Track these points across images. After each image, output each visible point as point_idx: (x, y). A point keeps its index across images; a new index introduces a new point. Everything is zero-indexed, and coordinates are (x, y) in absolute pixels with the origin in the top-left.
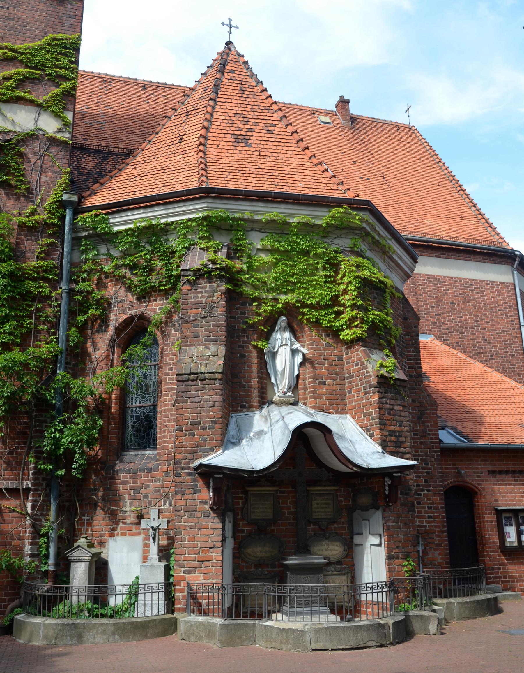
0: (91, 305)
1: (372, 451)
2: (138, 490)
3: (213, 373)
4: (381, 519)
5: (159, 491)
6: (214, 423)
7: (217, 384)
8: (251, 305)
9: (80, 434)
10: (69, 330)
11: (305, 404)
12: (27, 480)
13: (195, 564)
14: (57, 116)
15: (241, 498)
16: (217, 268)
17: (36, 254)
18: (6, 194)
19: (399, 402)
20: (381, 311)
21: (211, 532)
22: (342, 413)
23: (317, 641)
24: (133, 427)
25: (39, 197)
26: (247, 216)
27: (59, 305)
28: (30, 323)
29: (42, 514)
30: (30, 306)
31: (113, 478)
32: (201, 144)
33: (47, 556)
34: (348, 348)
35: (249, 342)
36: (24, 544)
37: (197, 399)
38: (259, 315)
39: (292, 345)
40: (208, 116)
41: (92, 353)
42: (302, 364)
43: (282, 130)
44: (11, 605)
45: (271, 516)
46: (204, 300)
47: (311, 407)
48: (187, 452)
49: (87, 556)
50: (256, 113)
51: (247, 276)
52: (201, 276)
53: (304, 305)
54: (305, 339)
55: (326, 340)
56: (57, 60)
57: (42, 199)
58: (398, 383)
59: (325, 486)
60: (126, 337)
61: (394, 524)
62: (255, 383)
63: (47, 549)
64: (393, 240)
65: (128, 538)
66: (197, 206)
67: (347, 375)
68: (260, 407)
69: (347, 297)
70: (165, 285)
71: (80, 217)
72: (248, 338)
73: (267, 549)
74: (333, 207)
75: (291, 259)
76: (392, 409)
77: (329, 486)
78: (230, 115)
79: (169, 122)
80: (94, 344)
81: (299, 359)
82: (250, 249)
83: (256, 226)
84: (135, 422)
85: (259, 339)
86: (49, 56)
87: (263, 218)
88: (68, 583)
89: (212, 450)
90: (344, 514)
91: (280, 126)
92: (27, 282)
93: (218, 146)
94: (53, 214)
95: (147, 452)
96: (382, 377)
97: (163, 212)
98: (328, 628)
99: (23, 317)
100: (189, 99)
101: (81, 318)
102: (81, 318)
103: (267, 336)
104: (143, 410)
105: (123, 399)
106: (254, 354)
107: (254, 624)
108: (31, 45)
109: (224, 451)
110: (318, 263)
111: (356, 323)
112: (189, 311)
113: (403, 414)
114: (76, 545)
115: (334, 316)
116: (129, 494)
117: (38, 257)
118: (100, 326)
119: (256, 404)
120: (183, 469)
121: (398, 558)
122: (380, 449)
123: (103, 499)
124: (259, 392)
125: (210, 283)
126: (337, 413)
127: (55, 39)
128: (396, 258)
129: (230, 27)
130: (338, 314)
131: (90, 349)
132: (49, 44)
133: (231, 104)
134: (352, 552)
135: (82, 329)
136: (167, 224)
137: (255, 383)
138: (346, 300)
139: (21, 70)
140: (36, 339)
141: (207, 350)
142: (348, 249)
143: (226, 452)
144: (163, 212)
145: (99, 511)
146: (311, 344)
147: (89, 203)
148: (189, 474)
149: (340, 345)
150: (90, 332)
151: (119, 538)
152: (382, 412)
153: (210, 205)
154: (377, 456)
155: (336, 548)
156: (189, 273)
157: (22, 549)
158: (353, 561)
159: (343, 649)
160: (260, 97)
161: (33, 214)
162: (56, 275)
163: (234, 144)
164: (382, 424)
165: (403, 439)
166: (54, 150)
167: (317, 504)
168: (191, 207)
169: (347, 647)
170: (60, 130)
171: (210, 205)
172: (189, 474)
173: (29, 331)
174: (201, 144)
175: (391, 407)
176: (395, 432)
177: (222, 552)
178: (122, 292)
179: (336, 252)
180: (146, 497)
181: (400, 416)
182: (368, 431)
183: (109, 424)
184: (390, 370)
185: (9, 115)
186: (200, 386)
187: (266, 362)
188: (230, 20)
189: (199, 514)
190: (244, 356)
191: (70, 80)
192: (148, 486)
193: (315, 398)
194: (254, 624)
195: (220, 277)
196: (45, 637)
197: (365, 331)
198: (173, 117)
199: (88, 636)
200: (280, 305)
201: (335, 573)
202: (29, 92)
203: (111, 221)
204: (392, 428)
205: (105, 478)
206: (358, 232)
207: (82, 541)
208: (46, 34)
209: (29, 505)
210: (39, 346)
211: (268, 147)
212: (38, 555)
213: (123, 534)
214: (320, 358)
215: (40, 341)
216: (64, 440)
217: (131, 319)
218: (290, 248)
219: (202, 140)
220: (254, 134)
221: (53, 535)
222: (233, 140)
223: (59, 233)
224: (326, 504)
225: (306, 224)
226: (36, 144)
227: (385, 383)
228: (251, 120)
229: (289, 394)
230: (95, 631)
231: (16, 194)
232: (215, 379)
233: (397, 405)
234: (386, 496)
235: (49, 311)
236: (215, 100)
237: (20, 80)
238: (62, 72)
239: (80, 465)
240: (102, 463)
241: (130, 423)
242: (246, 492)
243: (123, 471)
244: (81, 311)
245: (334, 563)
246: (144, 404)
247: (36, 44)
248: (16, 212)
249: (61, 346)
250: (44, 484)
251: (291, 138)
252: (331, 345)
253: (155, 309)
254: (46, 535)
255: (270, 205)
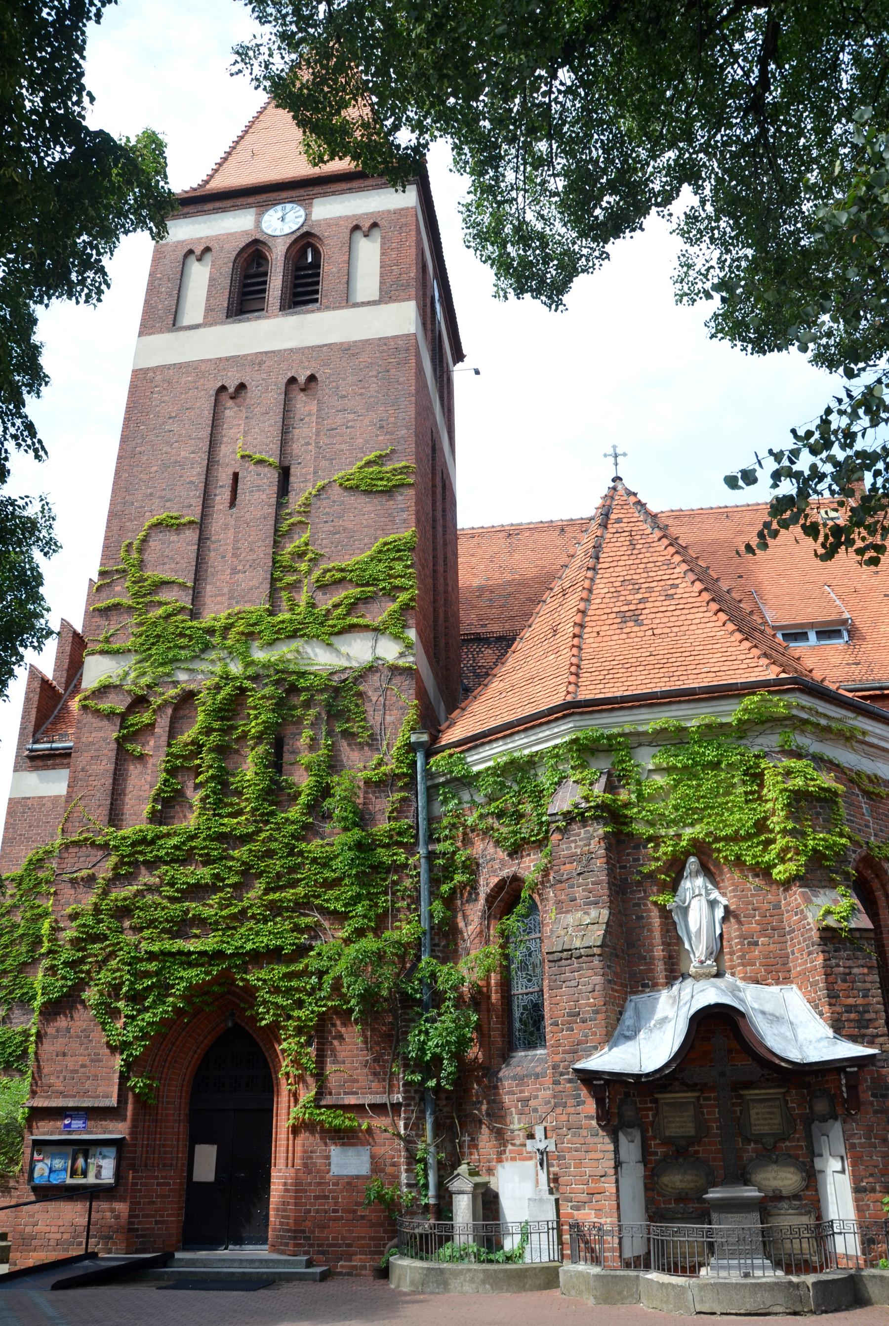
0: (457, 869)
1: (819, 1036)
2: (525, 1101)
3: (590, 947)
4: (841, 1134)
5: (549, 1102)
6: (596, 1012)
7: (596, 961)
8: (645, 847)
9: (448, 1035)
10: (431, 904)
11: (733, 974)
12: (398, 1093)
13: (584, 1197)
14: (397, 637)
15: (650, 1109)
16: (591, 807)
17: (387, 814)
18: (349, 745)
19: (861, 962)
20: (829, 832)
21: (601, 1155)
22: (786, 984)
23: (702, 1301)
24: (521, 1020)
25: (385, 743)
26: (628, 729)
27: (419, 873)
28: (386, 901)
29: (417, 1135)
30: (385, 880)
31: (496, 1087)
32: (575, 636)
33: (426, 1186)
34: (786, 890)
35: (646, 898)
36: (399, 1171)
37: (573, 983)
38: (658, 859)
39: (708, 894)
40: (585, 594)
41: (464, 929)
42: (725, 919)
43: (687, 590)
44: (390, 1244)
45: (692, 1132)
46: (579, 851)
47: (741, 978)
48: (565, 1052)
49: (469, 1187)
50: (651, 574)
51: (635, 810)
52: (573, 819)
53: (717, 839)
54: (727, 883)
55: (754, 882)
56: (391, 568)
57: (388, 744)
58: (857, 935)
59: (764, 1088)
60: (502, 904)
61: (863, 1140)
62: (658, 952)
63: (426, 1176)
64: (860, 718)
65: (518, 1163)
66: (563, 728)
67: (788, 929)
68: (670, 982)
69: (775, 819)
70: (538, 834)
71: (432, 761)
72: (645, 892)
73: (688, 1177)
74: (745, 695)
75: (695, 776)
76: (850, 973)
77: (770, 1088)
78: (615, 584)
79: (545, 607)
80: (465, 917)
81: (720, 913)
82: (638, 773)
83: (643, 739)
84: (522, 1014)
85: (661, 891)
86: (381, 566)
87: (649, 728)
88: (451, 1219)
89: (595, 1048)
90: (800, 1127)
91: (684, 585)
92: (379, 850)
93: (598, 633)
94: (402, 762)
95: (539, 1052)
96: (827, 929)
97: (525, 741)
98: (715, 1284)
99: (377, 893)
100: (567, 571)
101: (445, 888)
102: (445, 888)
103: (674, 887)
104: (531, 997)
105: (506, 985)
106: (655, 913)
107: (638, 1276)
108: (358, 558)
109: (610, 1049)
110: (733, 776)
111: (789, 856)
112: (562, 867)
113: (868, 978)
114: (456, 1172)
115: (761, 847)
116: (516, 1107)
117: (389, 818)
118: (470, 894)
119: (662, 980)
120: (562, 1074)
121: (873, 1190)
122: (830, 1033)
123: (488, 1115)
124: (665, 964)
125: (584, 827)
126: (777, 984)
127: (385, 544)
128: (875, 741)
129: (616, 456)
130: (769, 842)
131: (461, 924)
132: (380, 552)
133: (617, 569)
134: (816, 1181)
135: (449, 902)
136: (532, 756)
137: (658, 952)
138: (777, 822)
139: (351, 591)
140: (395, 918)
141: (586, 917)
142: (777, 749)
143: (615, 1049)
144: (525, 741)
145: (485, 1130)
146: (734, 891)
147: (447, 739)
148: (570, 1081)
149: (774, 887)
150: (459, 902)
151: (508, 1165)
152: (831, 979)
153: (578, 724)
154: (825, 1043)
155: (789, 1175)
156: (557, 818)
157: (398, 1177)
158: (818, 1195)
159: (736, 1314)
160: (658, 549)
161: (379, 765)
162: (412, 837)
163: (620, 626)
164: (833, 996)
165: (872, 1016)
166: (397, 680)
167: (757, 1114)
168: (556, 730)
169: (742, 1311)
170: (402, 655)
171: (578, 724)
172: (570, 1081)
173: (386, 911)
174: (575, 636)
175: (847, 971)
176: (856, 1006)
177: (617, 1181)
178: (491, 849)
179: (757, 757)
180: (535, 1110)
181: (865, 982)
182: (816, 1007)
183: (489, 1018)
184: (842, 917)
185: (344, 649)
186: (576, 965)
187: (674, 923)
188: (614, 447)
189: (584, 1132)
190: (642, 917)
191: (407, 589)
192: (536, 1097)
193: (744, 965)
194: (638, 1276)
195: (596, 818)
196: (412, 1283)
197: (801, 865)
198: (549, 600)
199: (455, 1284)
200: (684, 843)
201: (791, 1211)
202: (362, 616)
203: (469, 760)
204: (851, 1001)
205: (489, 1088)
206: (787, 722)
207: (463, 1169)
208: (376, 539)
209: (402, 1124)
210: (399, 928)
211: (666, 620)
212: (416, 1185)
213: (513, 1159)
214: (747, 909)
215: (400, 921)
216: (430, 1043)
217: (503, 881)
218: (690, 762)
219: (577, 630)
220: (648, 605)
221: (431, 1160)
222: (619, 620)
223: (411, 785)
224: (770, 1113)
225: (709, 726)
226: (376, 677)
227: (833, 937)
228: (644, 586)
229: (709, 962)
230: (462, 1277)
231: (360, 743)
232: (594, 955)
233: (858, 967)
234: (846, 1101)
235: (407, 883)
236: (594, 569)
237: (352, 604)
238: (397, 582)
239: (449, 1074)
240: (483, 1069)
241: (517, 1015)
242: (656, 1101)
243: (508, 1078)
244: (446, 878)
245: (788, 1198)
246: (531, 990)
247: (364, 556)
248: (361, 765)
249: (425, 925)
250: (417, 1097)
251: (699, 599)
252: (762, 889)
253: (529, 867)
254: (423, 1160)
255: (656, 709)
